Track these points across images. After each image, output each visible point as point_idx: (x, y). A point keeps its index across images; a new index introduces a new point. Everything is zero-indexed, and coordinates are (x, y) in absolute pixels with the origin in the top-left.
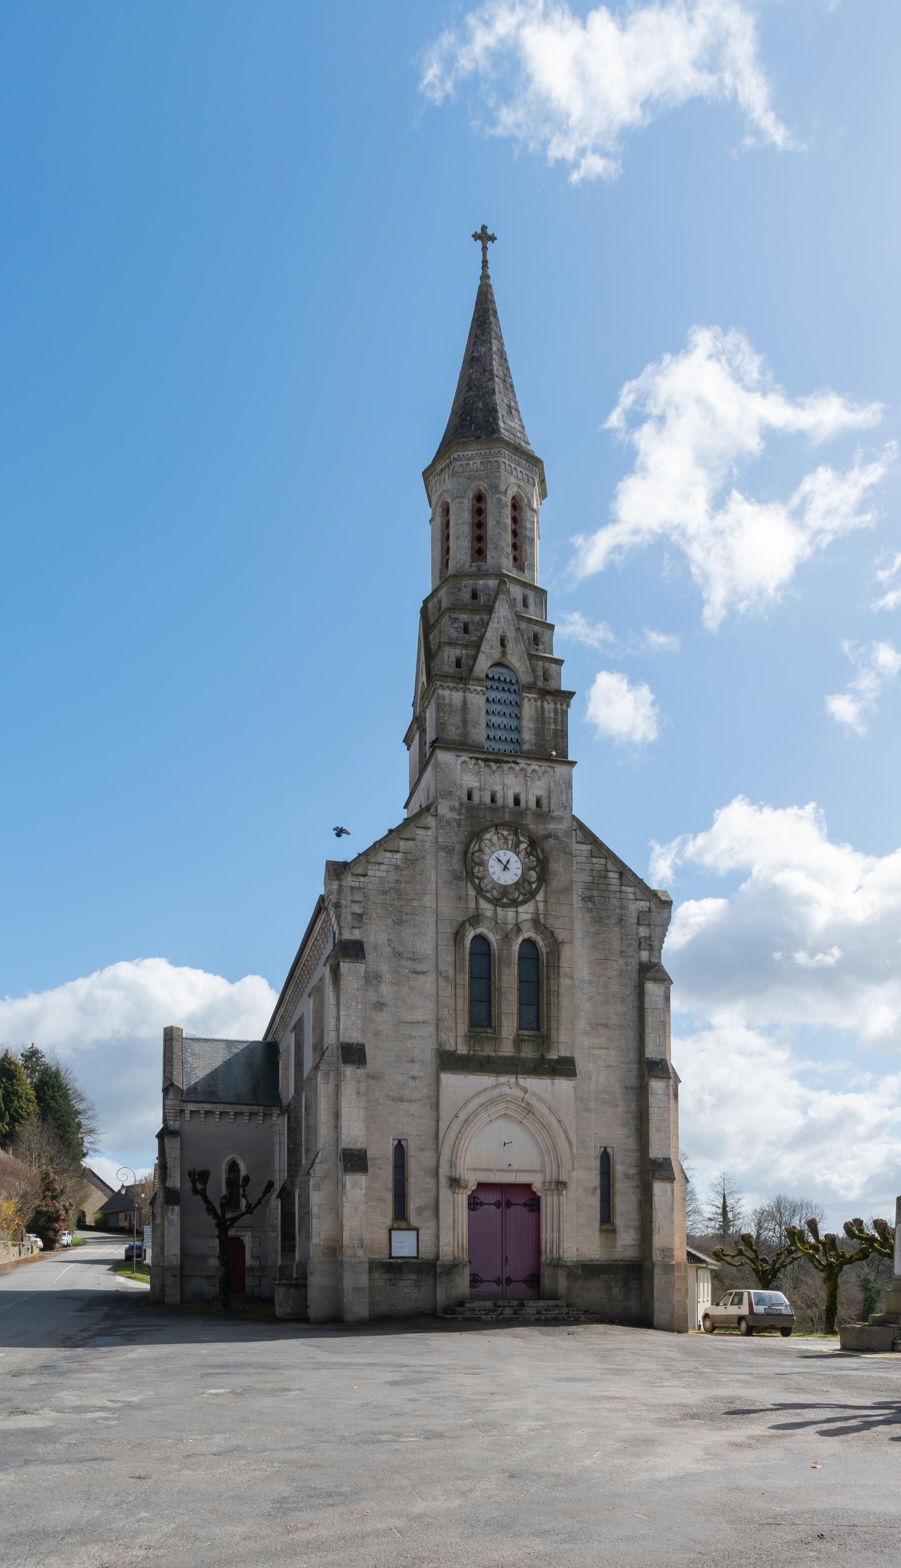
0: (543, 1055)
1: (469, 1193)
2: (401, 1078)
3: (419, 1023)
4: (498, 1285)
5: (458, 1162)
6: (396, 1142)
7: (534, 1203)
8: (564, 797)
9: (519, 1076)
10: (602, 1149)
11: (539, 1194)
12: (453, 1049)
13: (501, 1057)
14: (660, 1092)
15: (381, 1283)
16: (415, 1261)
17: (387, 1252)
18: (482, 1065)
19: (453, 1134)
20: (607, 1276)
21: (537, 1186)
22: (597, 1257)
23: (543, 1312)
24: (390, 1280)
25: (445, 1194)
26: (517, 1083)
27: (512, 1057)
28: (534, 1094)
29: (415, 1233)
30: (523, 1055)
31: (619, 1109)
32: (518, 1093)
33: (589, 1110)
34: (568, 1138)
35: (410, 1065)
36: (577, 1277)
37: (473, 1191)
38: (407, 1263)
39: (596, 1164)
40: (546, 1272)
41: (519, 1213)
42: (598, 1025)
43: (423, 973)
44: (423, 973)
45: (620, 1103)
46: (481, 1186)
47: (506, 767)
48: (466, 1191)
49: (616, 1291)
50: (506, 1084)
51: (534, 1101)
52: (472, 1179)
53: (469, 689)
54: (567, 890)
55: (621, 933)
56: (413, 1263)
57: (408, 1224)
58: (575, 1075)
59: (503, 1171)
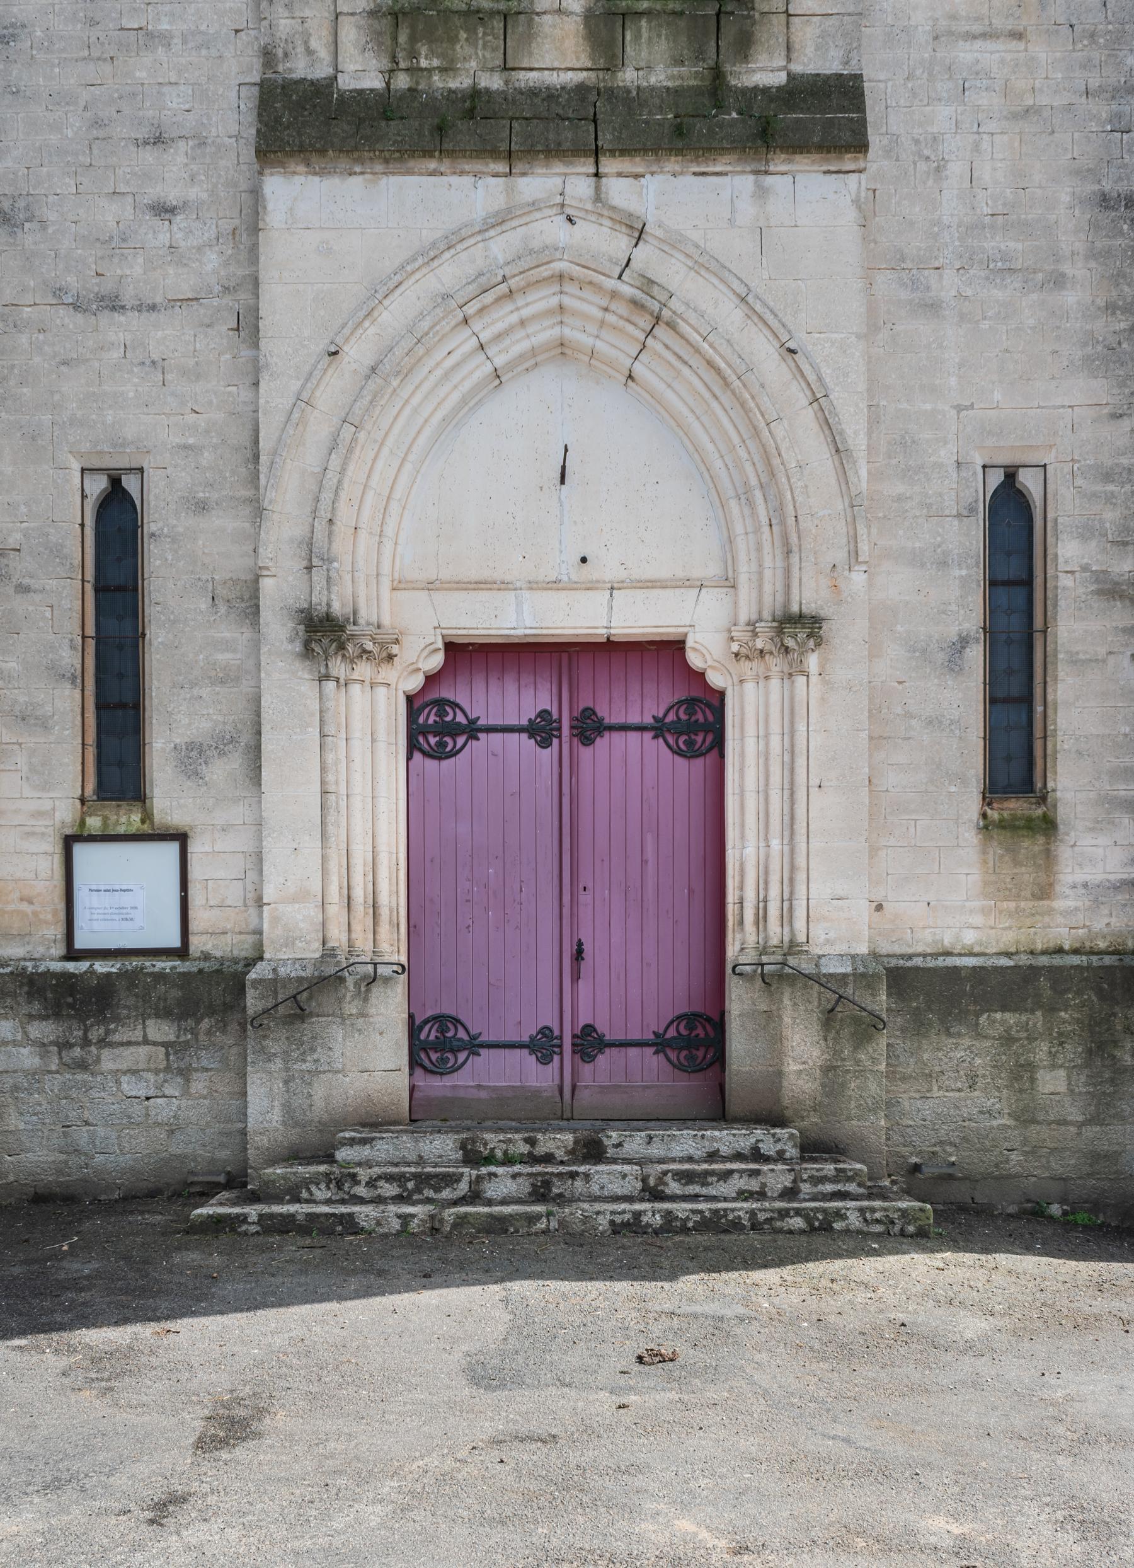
0: (717, 74)
1: (415, 683)
2: (110, 215)
4: (545, 1060)
5: (337, 547)
6: (98, 485)
7: (698, 723)
9: (609, 165)
10: (996, 479)
11: (715, 679)
12: (322, 71)
13: (533, 92)
16: (164, 965)
17: (57, 931)
18: (441, 130)
19: (319, 427)
20: (1011, 1018)
21: (707, 652)
22: (969, 938)
23: (674, 1187)
25: (286, 683)
26: (598, 198)
27: (581, 89)
28: (673, 243)
29: (174, 848)
30: (628, 77)
31: (1071, 298)
33: (932, 308)
34: (827, 424)
35: (149, 155)
36: (868, 1027)
37: (431, 679)
38: (131, 978)
39: (968, 539)
40: (740, 1000)
41: (633, 766)
45: (1076, 270)
46: (461, 654)
48: (388, 673)
49: (1052, 1082)
50: (550, 205)
51: (673, 273)
56: (160, 977)
57: (147, 817)
58: (860, 146)
59: (555, 585)
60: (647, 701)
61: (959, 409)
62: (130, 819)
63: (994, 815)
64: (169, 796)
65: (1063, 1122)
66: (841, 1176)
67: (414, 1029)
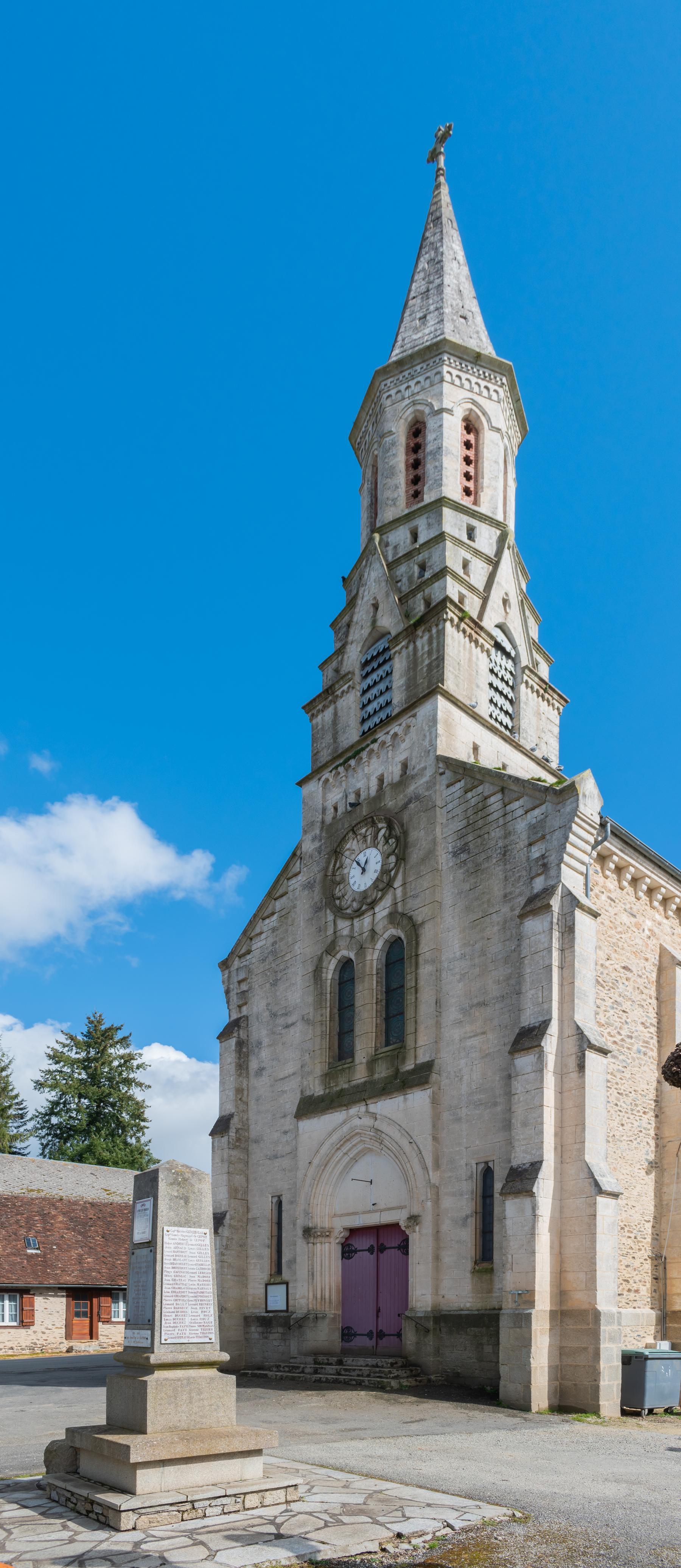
0: (397, 1070)
3: (289, 1076)
8: (426, 743)
9: (369, 1102)
14: (529, 1069)
15: (256, 1336)
17: (264, 1306)
20: (476, 1329)
22: (468, 1305)
24: (263, 1333)
30: (376, 1076)
32: (367, 1121)
35: (283, 1120)
37: (347, 1239)
42: (472, 1006)
43: (293, 1024)
44: (293, 1024)
46: (354, 1232)
47: (364, 754)
51: (384, 1127)
52: (340, 1225)
53: (337, 696)
54: (430, 854)
55: (505, 871)
56: (281, 1317)
60: (393, 1241)
61: (467, 1148)
62: (278, 1280)
63: (477, 1268)
64: (286, 1275)
65: (491, 1361)
66: (380, 1372)
67: (343, 1330)
